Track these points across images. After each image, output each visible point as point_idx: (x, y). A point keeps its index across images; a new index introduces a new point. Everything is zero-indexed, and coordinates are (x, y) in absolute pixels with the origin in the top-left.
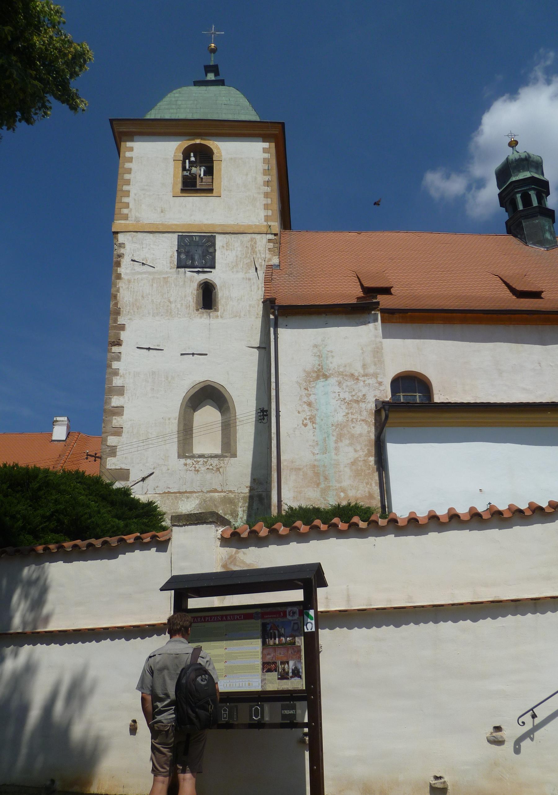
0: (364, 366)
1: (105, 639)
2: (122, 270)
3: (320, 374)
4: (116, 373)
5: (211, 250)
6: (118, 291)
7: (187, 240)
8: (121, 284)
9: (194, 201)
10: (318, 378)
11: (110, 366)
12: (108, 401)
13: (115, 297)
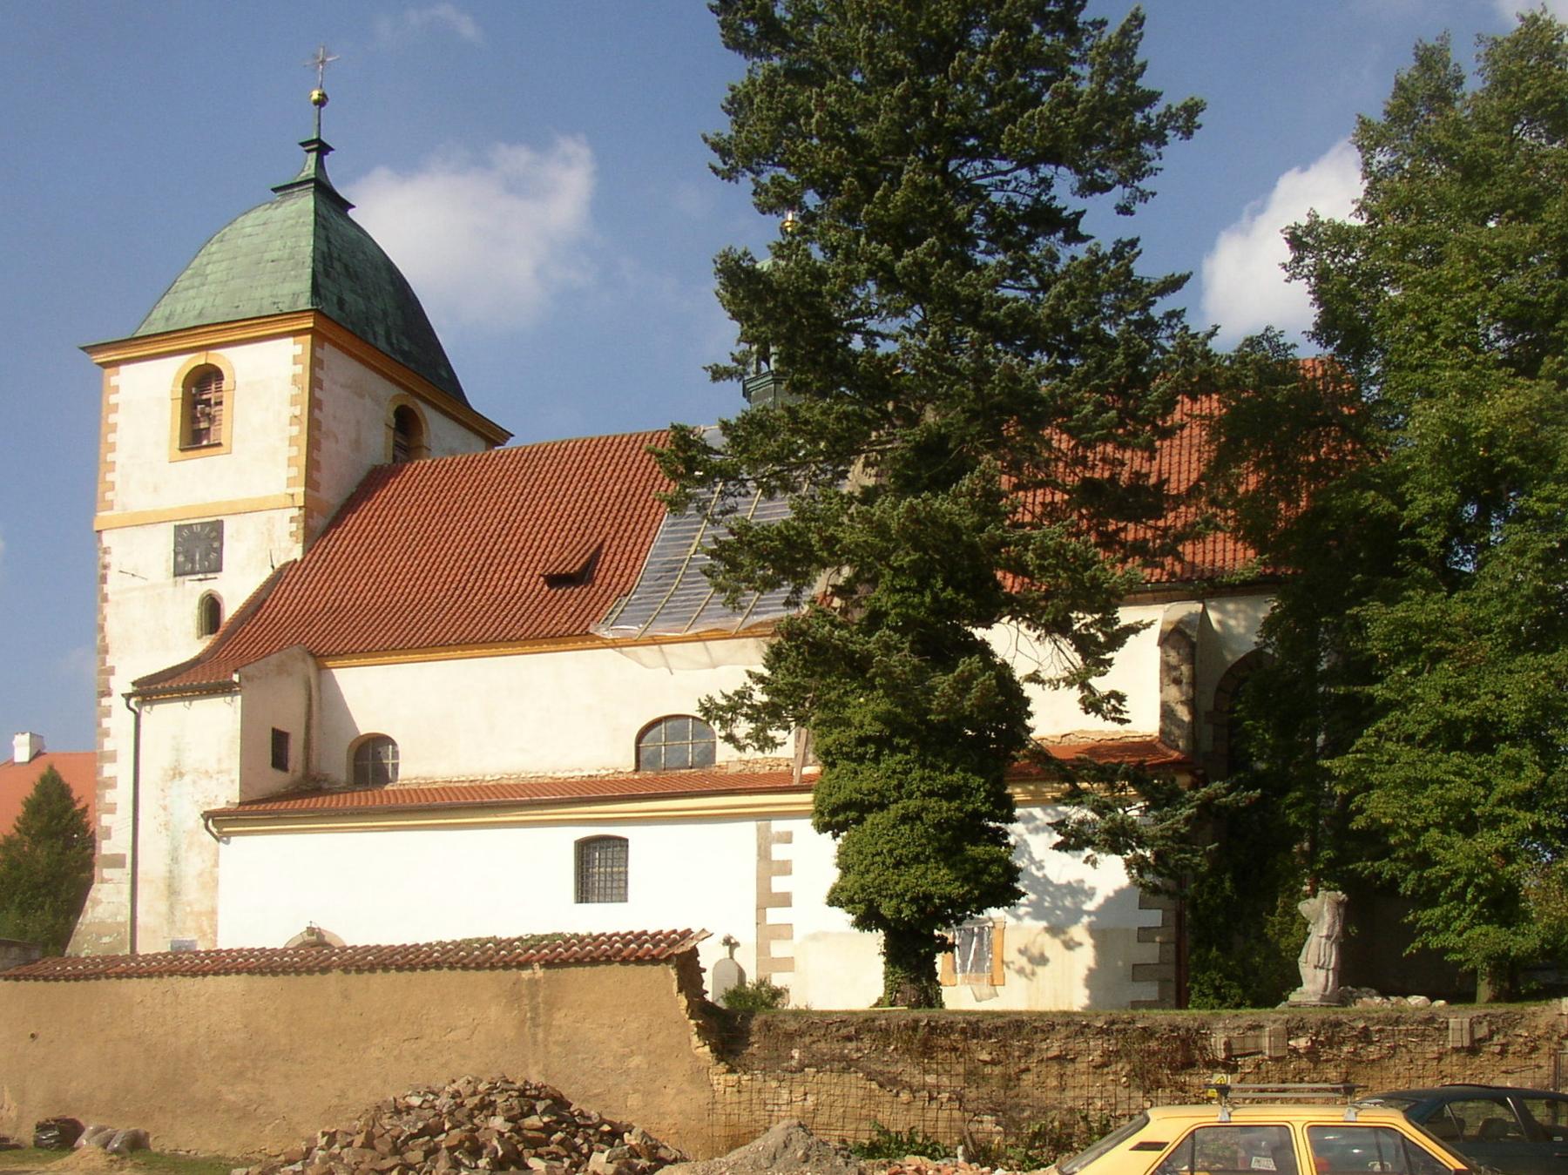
0: (219, 761)
1: (1090, 998)
2: (108, 588)
3: (177, 773)
4: (106, 734)
5: (216, 545)
6: (105, 619)
7: (185, 533)
8: (109, 609)
9: (199, 464)
10: (174, 777)
11: (100, 725)
12: (99, 771)
13: (102, 628)
